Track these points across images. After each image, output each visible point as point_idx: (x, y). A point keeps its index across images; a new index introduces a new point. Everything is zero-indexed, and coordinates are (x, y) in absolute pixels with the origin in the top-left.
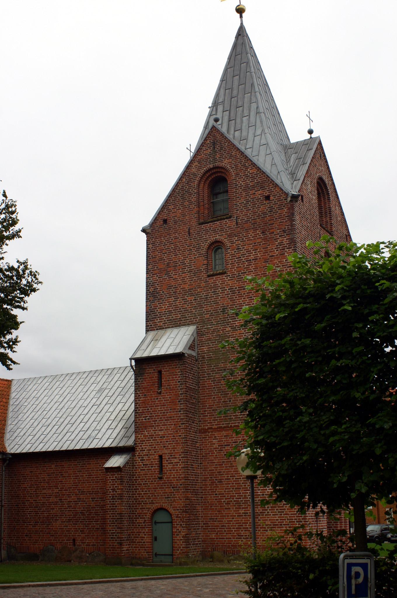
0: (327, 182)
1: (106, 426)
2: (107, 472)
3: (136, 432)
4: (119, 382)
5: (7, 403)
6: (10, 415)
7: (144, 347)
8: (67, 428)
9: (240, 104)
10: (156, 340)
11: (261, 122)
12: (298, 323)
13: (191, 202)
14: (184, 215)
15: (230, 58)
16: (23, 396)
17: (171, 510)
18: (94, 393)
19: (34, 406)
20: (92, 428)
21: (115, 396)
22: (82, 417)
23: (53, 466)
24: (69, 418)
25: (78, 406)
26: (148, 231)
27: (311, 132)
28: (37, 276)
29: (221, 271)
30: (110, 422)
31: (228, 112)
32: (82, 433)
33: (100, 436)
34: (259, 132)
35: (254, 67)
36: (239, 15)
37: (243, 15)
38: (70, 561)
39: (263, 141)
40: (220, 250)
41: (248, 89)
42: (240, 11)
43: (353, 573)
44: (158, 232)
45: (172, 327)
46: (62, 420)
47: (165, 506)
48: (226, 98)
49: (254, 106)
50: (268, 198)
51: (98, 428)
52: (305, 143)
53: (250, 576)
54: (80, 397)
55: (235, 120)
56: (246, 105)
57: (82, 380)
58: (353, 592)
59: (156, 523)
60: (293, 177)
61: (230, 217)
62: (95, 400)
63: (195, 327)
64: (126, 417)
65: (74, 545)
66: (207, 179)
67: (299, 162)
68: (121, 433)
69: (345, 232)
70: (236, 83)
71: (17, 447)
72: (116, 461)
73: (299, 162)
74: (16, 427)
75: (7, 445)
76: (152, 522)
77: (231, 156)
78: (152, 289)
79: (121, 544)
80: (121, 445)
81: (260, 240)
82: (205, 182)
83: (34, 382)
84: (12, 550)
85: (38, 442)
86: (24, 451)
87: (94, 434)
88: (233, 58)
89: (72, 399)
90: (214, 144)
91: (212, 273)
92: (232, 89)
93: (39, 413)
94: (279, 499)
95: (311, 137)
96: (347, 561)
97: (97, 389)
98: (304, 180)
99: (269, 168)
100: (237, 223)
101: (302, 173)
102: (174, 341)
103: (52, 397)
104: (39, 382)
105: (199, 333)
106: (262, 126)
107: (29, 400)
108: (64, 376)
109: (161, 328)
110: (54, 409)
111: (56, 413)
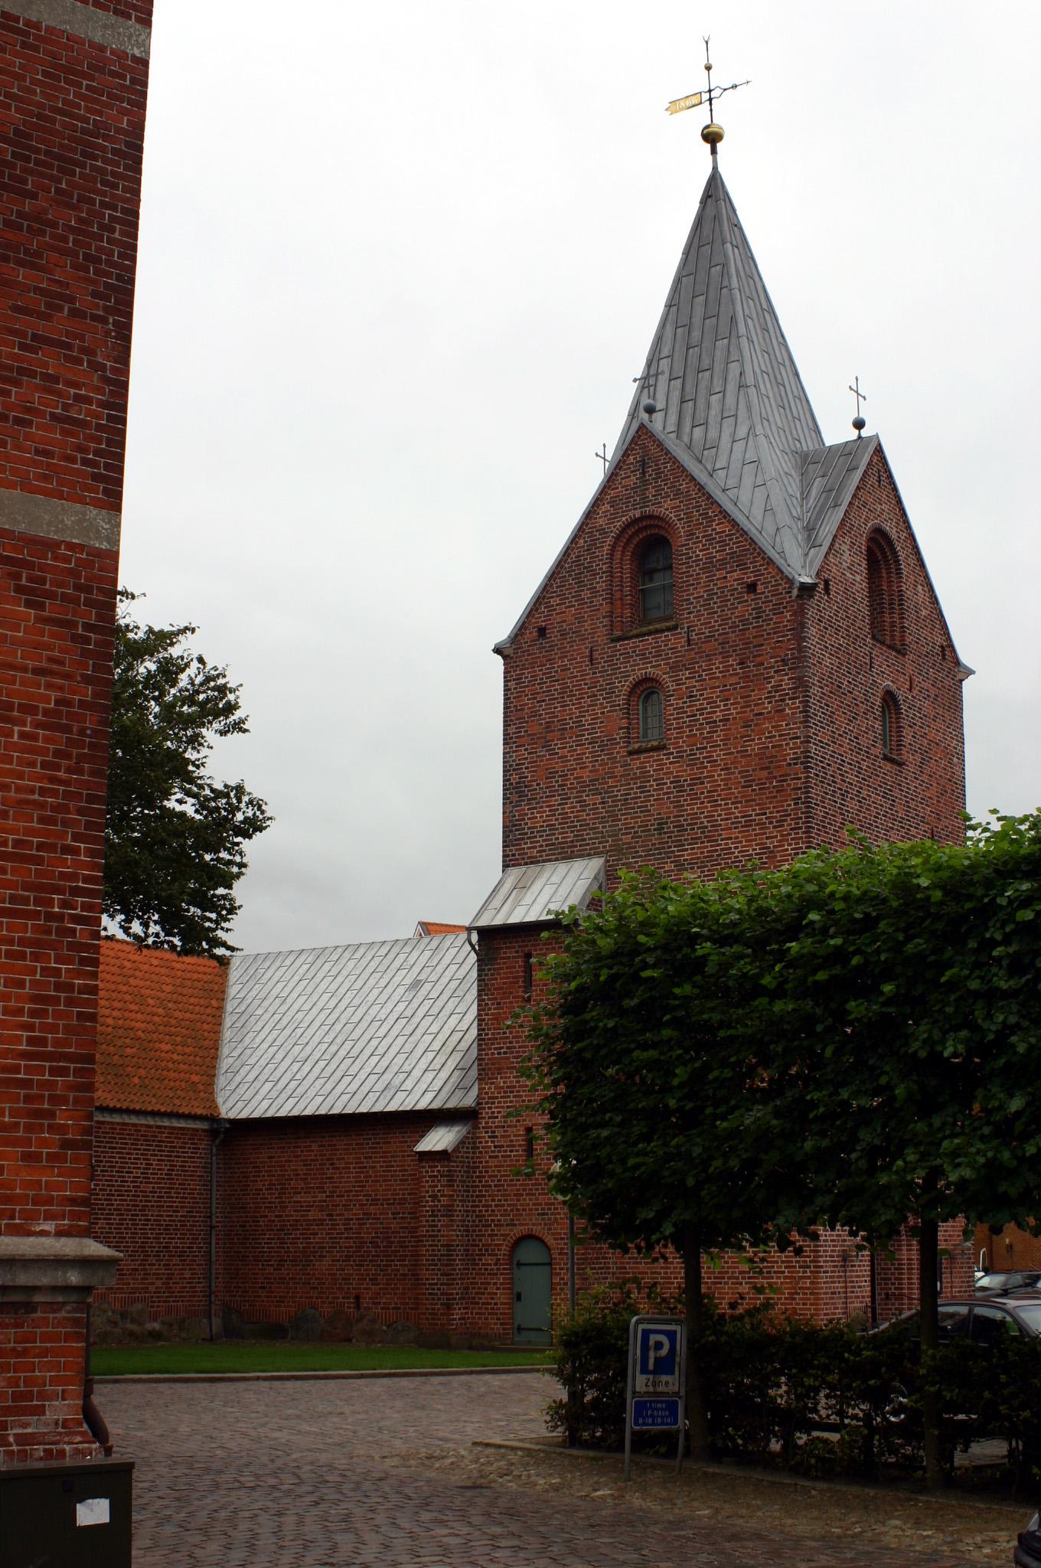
0: (894, 536)
1: (423, 1065)
2: (420, 1161)
3: (480, 1079)
4: (454, 968)
5: (221, 1009)
6: (227, 1034)
7: (496, 902)
8: (343, 1067)
9: (706, 362)
10: (521, 887)
11: (749, 408)
12: (607, 993)
13: (594, 592)
14: (581, 620)
15: (687, 252)
16: (254, 993)
17: (550, 1240)
18: (402, 989)
19: (277, 1017)
20: (394, 1068)
21: (445, 997)
22: (374, 1042)
23: (315, 1147)
24: (348, 1045)
25: (368, 1018)
26: (506, 652)
27: (859, 424)
28: (264, 807)
29: (655, 743)
30: (430, 1055)
31: (679, 381)
32: (373, 1078)
33: (408, 1085)
34: (742, 432)
35: (737, 271)
36: (708, 146)
37: (719, 145)
38: (350, 1340)
39: (751, 456)
40: (655, 696)
41: (724, 329)
42: (712, 138)
43: (651, 1343)
44: (528, 651)
45: (557, 860)
46: (333, 1048)
47: (537, 1230)
48: (677, 348)
49: (735, 369)
50: (752, 588)
51: (407, 1068)
52: (847, 451)
53: (560, 1353)
54: (371, 998)
55: (695, 400)
56: (718, 368)
57: (377, 960)
58: (651, 1367)
59: (519, 1264)
60: (809, 537)
61: (675, 627)
62: (402, 1006)
63: (595, 864)
64: (464, 1045)
65: (358, 1307)
66: (629, 540)
67: (827, 499)
68: (452, 1080)
69: (940, 640)
70: (699, 311)
71: (240, 1105)
72: (439, 1139)
73: (827, 499)
74: (239, 1063)
75: (220, 1100)
76: (511, 1264)
77: (678, 493)
78: (515, 779)
79: (449, 1307)
80: (450, 1105)
81: (733, 680)
82: (624, 548)
83: (278, 964)
84: (234, 1317)
85: (284, 1096)
86: (255, 1115)
87: (397, 1082)
88: (693, 251)
89: (356, 1002)
90: (644, 464)
91: (636, 746)
92: (689, 327)
93: (287, 1032)
94: (597, 1238)
95: (860, 437)
96: (641, 1327)
97: (408, 981)
98: (832, 545)
99: (760, 518)
100: (689, 640)
101: (828, 529)
102: (558, 889)
103: (315, 997)
104: (288, 962)
105: (609, 876)
106: (750, 417)
107: (266, 1003)
108: (340, 950)
109: (534, 861)
110: (317, 1023)
111: (321, 1033)
